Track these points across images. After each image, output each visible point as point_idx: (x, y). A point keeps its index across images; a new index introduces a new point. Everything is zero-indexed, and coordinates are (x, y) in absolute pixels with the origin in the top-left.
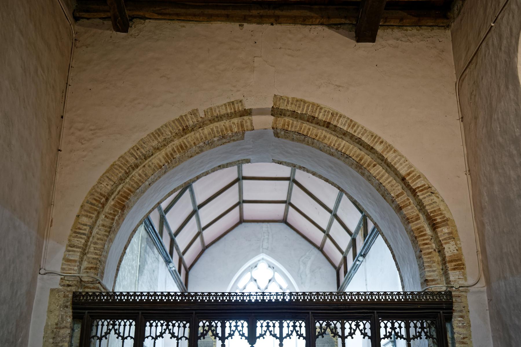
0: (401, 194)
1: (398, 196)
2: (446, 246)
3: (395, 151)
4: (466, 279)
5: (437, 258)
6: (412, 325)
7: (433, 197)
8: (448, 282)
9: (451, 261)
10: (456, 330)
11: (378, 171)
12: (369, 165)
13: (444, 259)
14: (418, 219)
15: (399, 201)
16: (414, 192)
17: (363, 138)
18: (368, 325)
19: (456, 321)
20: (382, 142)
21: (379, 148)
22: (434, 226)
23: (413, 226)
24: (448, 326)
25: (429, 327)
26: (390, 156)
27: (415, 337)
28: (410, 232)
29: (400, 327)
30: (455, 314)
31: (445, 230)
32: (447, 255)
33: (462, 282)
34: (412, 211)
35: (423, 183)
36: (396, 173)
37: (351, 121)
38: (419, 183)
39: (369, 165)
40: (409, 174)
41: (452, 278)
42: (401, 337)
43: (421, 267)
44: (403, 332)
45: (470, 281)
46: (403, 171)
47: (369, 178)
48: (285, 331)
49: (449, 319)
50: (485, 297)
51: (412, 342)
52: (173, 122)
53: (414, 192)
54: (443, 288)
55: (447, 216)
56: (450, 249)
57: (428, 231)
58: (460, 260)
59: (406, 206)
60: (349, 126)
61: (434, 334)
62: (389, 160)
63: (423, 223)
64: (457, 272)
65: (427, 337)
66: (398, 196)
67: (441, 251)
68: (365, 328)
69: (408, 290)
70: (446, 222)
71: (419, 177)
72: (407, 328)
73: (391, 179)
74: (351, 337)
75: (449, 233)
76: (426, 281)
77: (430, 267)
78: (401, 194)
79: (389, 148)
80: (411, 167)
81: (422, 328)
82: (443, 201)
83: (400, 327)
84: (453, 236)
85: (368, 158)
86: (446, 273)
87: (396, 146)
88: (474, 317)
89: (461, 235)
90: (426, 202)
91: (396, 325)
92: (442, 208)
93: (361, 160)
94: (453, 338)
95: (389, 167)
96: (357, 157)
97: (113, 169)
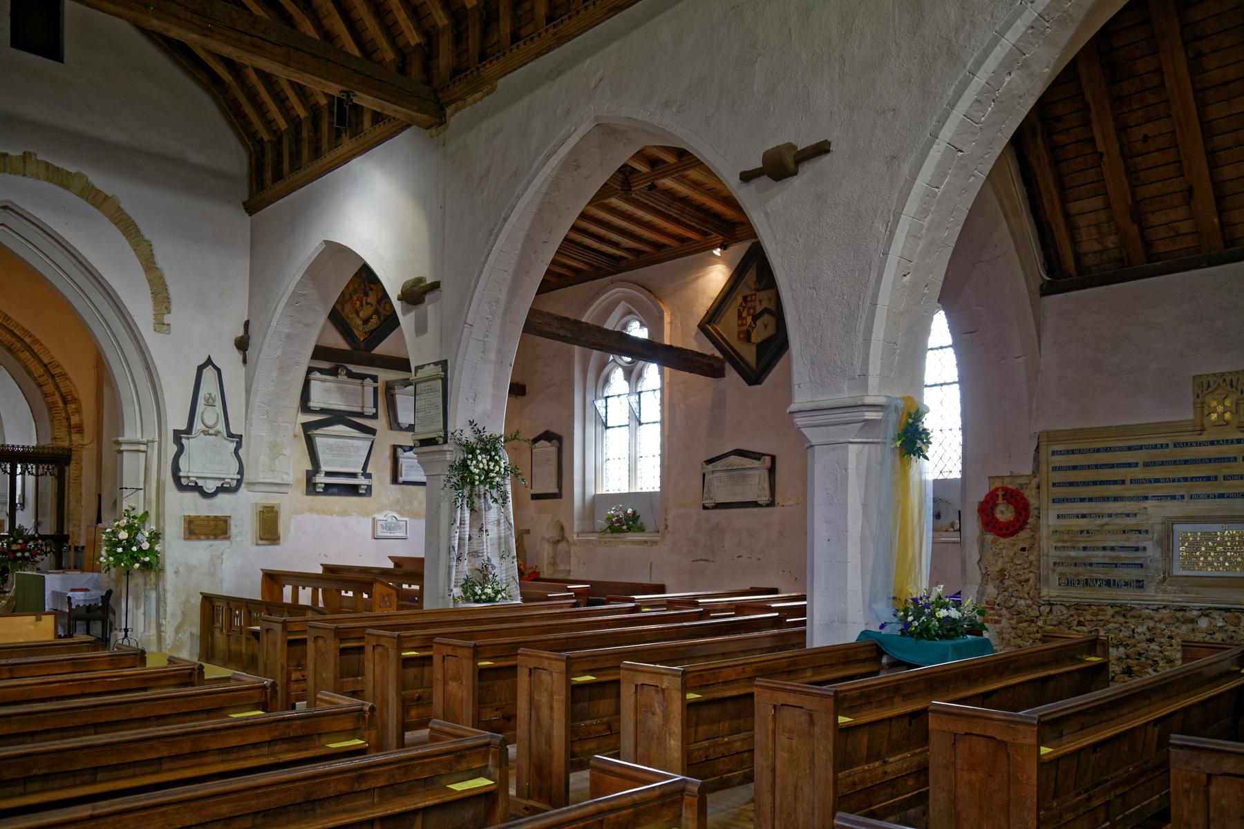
0: (43, 375)
1: (40, 377)
2: (72, 417)
3: (41, 344)
4: (83, 440)
5: (65, 423)
6: (41, 467)
7: (68, 382)
8: (71, 441)
9: (75, 428)
10: (72, 471)
11: (25, 355)
12: (18, 351)
13: (70, 425)
14: (54, 395)
15: (40, 380)
16: (53, 376)
17: (15, 331)
18: (8, 466)
19: (73, 466)
20: (31, 336)
21: (28, 340)
22: (65, 402)
23: (50, 400)
24: (67, 468)
25: (53, 468)
26: (36, 348)
27: (42, 475)
28: (47, 403)
29: (32, 468)
30: (72, 462)
31: (73, 406)
32: (72, 423)
33: (81, 442)
34: (50, 388)
35: (60, 371)
36: (40, 361)
37: (6, 315)
38: (57, 371)
39: (18, 351)
40: (50, 363)
41: (73, 439)
42: (32, 474)
43: (53, 427)
44: (34, 471)
45: (86, 442)
46: (46, 361)
47: (18, 359)
48: (40, 471)
49: (68, 464)
50: (95, 452)
51: (40, 478)
52: (257, 666)
53: (53, 376)
54: (66, 444)
55: (76, 396)
56: (75, 419)
57: (61, 404)
58: (82, 427)
59: (46, 384)
60: (4, 319)
61: (56, 474)
62: (35, 350)
63: (58, 398)
64: (78, 435)
65: (51, 475)
66: (40, 377)
67: (68, 419)
68: (5, 468)
69: (42, 444)
70: (75, 400)
71: (58, 366)
72: (37, 469)
73: (35, 363)
74: (930, 351)
75: (76, 409)
76: (55, 438)
77: (59, 429)
78: (43, 375)
79: (36, 341)
80: (52, 358)
81: (48, 469)
82: (74, 385)
83: (32, 468)
84: (78, 411)
85: (18, 345)
86: (70, 433)
87: (43, 341)
88: (85, 464)
89: (84, 410)
90: (61, 385)
91: (29, 466)
92: (73, 390)
93: (12, 345)
94: (69, 476)
95: (35, 355)
96: (9, 342)
97: (682, 805)
